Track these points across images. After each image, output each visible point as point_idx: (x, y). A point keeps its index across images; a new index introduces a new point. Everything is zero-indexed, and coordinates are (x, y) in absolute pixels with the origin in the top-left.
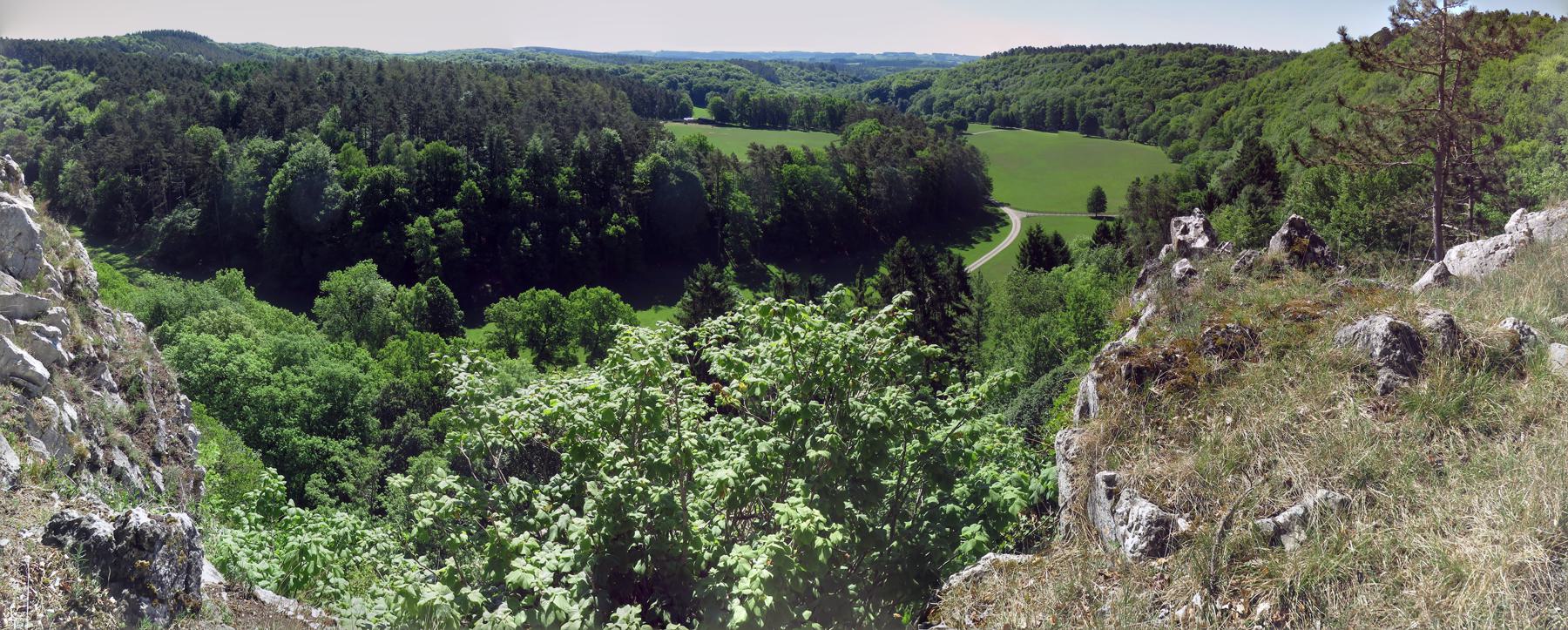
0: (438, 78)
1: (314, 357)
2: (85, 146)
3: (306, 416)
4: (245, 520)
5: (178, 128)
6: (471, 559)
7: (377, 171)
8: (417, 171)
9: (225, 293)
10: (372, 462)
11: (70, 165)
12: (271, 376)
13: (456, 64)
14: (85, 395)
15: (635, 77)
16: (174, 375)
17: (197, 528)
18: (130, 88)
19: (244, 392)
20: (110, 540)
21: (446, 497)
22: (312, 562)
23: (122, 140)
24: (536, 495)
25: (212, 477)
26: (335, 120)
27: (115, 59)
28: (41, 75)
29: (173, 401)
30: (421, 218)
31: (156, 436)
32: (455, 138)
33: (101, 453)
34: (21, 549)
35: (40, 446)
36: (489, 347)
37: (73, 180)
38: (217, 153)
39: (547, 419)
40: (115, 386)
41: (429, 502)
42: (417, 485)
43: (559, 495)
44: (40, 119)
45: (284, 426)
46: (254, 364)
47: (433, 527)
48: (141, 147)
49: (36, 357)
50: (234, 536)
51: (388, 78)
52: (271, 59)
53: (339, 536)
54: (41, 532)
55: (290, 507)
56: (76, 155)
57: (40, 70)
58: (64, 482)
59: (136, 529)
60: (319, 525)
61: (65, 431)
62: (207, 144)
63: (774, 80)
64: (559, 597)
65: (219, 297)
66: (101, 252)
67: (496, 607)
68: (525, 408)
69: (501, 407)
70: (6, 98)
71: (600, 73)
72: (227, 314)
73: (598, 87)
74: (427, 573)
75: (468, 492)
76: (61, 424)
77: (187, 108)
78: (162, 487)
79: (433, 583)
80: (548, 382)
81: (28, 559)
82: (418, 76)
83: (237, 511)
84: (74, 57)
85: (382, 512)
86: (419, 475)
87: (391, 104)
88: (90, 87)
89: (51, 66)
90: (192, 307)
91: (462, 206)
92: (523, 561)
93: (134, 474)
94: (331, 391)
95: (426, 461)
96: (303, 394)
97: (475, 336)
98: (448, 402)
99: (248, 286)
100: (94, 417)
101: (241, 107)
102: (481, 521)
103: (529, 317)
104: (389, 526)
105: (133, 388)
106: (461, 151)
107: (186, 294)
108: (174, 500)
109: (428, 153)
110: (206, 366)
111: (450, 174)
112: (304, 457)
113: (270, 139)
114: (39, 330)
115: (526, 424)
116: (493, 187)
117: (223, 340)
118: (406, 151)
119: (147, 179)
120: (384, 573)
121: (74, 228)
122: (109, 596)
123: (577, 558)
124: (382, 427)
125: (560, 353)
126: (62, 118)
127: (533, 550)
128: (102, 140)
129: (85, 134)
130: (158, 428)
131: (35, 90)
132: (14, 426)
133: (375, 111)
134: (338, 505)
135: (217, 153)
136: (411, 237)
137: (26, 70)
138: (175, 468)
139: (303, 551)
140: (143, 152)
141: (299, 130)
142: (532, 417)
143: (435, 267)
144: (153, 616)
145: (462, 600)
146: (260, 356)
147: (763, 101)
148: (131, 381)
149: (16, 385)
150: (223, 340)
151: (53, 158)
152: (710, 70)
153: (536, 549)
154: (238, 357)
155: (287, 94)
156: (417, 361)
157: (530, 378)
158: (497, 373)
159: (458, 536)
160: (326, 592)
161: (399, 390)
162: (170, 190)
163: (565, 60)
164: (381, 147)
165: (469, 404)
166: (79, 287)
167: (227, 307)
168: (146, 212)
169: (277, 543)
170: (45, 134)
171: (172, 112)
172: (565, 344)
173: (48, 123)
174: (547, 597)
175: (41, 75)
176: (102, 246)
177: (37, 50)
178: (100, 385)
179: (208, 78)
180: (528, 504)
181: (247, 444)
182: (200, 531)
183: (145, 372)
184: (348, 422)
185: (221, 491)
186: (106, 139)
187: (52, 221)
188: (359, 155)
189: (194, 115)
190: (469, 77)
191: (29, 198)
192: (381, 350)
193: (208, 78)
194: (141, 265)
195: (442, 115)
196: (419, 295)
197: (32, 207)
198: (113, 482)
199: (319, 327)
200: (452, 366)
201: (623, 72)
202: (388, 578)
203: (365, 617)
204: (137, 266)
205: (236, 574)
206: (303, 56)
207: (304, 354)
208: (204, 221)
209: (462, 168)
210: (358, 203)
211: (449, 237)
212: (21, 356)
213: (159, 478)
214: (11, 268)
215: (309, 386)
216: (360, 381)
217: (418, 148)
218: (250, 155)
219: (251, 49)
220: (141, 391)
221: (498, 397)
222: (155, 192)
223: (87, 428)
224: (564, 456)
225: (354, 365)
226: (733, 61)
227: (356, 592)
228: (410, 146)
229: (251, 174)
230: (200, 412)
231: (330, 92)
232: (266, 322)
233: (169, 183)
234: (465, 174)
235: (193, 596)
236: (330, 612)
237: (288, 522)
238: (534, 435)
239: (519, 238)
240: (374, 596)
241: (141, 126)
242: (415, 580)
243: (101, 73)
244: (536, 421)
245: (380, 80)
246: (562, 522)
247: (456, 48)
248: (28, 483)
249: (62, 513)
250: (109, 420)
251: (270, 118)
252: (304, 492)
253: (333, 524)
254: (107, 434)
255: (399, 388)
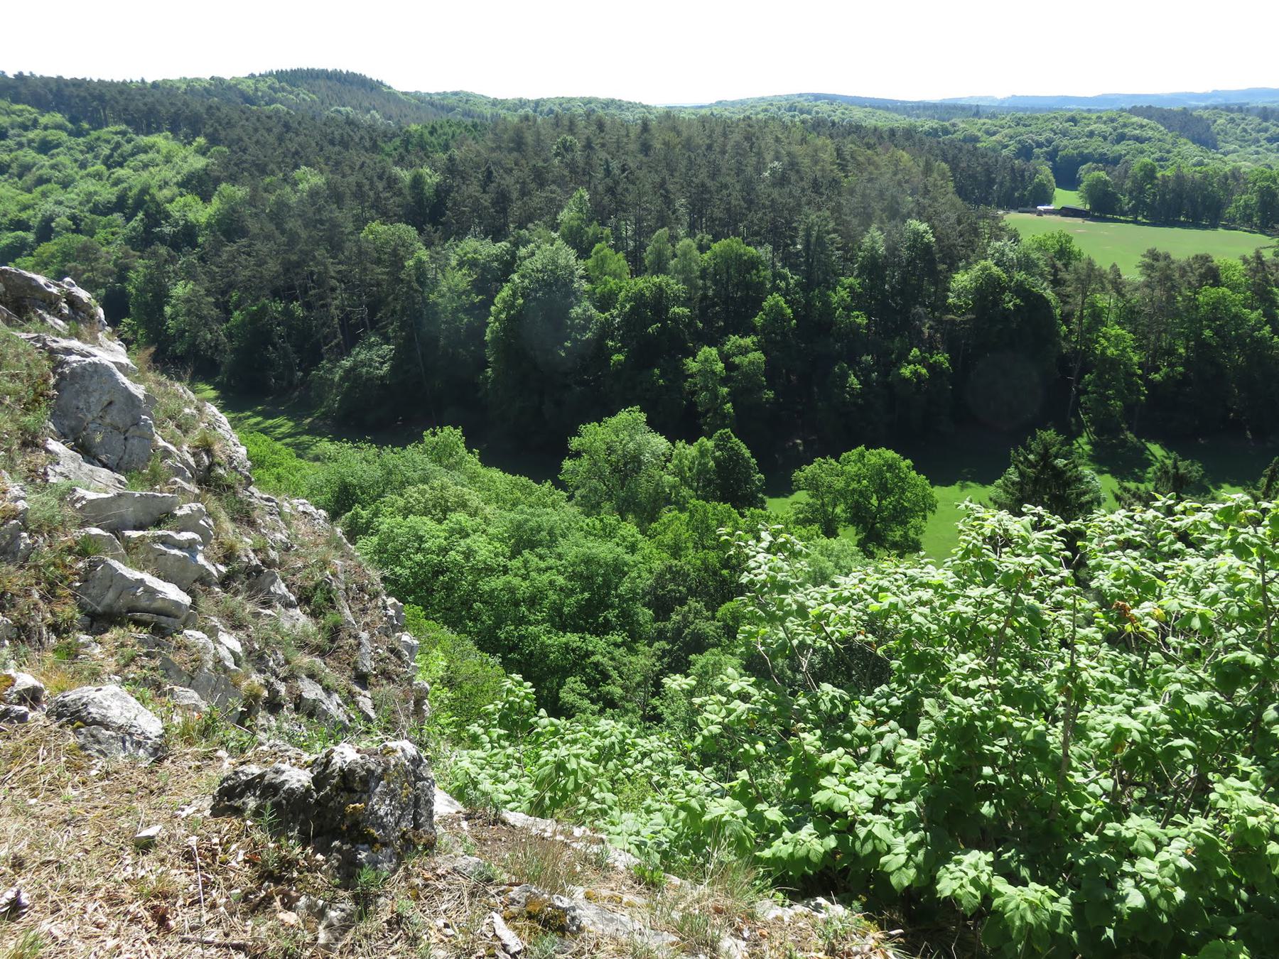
0: (730, 144)
1: (564, 536)
2: (202, 259)
3: (557, 609)
4: (485, 738)
5: (350, 227)
6: (769, 774)
7: (643, 284)
8: (700, 282)
9: (438, 460)
10: (643, 661)
11: (180, 290)
12: (509, 563)
13: (758, 121)
14: (250, 618)
15: (965, 140)
16: (375, 575)
17: (423, 755)
18: (266, 165)
19: (474, 586)
20: (308, 790)
21: (738, 702)
22: (572, 778)
23: (262, 247)
24: (854, 708)
25: (438, 693)
26: (581, 210)
27: (235, 116)
28: (108, 142)
29: (377, 607)
30: (706, 348)
31: (358, 654)
32: (757, 234)
33: (282, 688)
34: (181, 832)
35: (190, 696)
36: (797, 522)
37: (189, 313)
38: (411, 263)
39: (874, 617)
40: (293, 598)
41: (717, 708)
42: (702, 687)
43: (885, 709)
44: (117, 217)
45: (529, 623)
46: (484, 549)
47: (721, 735)
48: (294, 258)
49: (166, 579)
50: (472, 758)
51: (657, 145)
52: (481, 116)
53: (604, 747)
54: (208, 803)
55: (541, 717)
56: (188, 273)
57: (105, 132)
58: (233, 734)
59: (341, 769)
60: (578, 735)
61: (226, 669)
62: (395, 250)
63: (1206, 140)
64: (879, 825)
65: (430, 466)
66: (248, 417)
67: (800, 828)
68: (845, 601)
69: (812, 598)
70: (48, 181)
71: (909, 133)
72: (443, 488)
73: (906, 156)
74: (714, 786)
75: (767, 697)
76: (219, 661)
77: (359, 194)
78: (372, 714)
79: (722, 797)
80: (877, 570)
81: (193, 841)
82: (702, 141)
83: (474, 728)
84: (163, 112)
85: (658, 718)
86: (704, 676)
87: (663, 184)
88: (199, 163)
89: (123, 127)
90: (393, 482)
91: (764, 331)
92: (835, 780)
93: (333, 705)
94: (588, 578)
95: (712, 659)
96: (551, 583)
97: (778, 507)
98: (741, 590)
99: (469, 449)
100: (267, 644)
101: (442, 192)
102: (782, 732)
103: (854, 485)
104: (666, 734)
105: (318, 597)
106: (764, 252)
107: (383, 466)
108: (391, 727)
109: (715, 256)
110: (419, 557)
111: (748, 286)
112: (556, 658)
113: (488, 240)
114: (165, 541)
115: (845, 620)
116: (809, 305)
117: (440, 522)
118: (685, 254)
119: (308, 306)
120: (659, 786)
121: (201, 386)
122: (315, 853)
123: (905, 786)
124: (656, 620)
125: (897, 534)
126: (157, 215)
127: (848, 770)
128: (230, 248)
129: (200, 240)
130: (360, 644)
131: (100, 167)
132: (145, 679)
133: (640, 195)
134: (601, 712)
135: (411, 263)
136: (692, 376)
137: (79, 133)
138: (388, 689)
139: (560, 766)
140: (298, 264)
141: (530, 225)
142: (853, 613)
143: (725, 416)
144: (375, 864)
145: (758, 818)
146: (492, 539)
147: (1180, 178)
148: (315, 588)
149: (137, 623)
150: (440, 522)
151: (149, 280)
152: (1091, 128)
153: (853, 769)
154: (462, 542)
155: (509, 171)
156: (701, 538)
157: (853, 564)
158: (808, 555)
159: (753, 747)
160: (590, 808)
161: (677, 575)
162: (345, 321)
163: (858, 114)
164: (649, 249)
165: (770, 592)
166: (221, 471)
167: (442, 478)
168: (312, 356)
169: (526, 760)
170: (129, 241)
171: (337, 202)
172: (904, 523)
173: (133, 223)
174: (864, 823)
175: (108, 142)
176: (249, 409)
177: (94, 98)
178: (271, 601)
179: (388, 148)
180: (844, 716)
181: (481, 648)
182: (427, 758)
183: (334, 575)
184: (611, 615)
185: (451, 708)
186: (235, 247)
187: (163, 378)
188: (618, 261)
189: (372, 207)
190: (777, 140)
191: (118, 346)
192: (653, 525)
193: (388, 148)
194: (312, 431)
195: (736, 200)
196: (703, 453)
197: (124, 359)
198: (304, 720)
199: (570, 498)
200: (747, 545)
201: (946, 132)
202: (666, 792)
203: (638, 833)
204: (307, 432)
205: (477, 799)
206: (531, 112)
207: (551, 533)
208: (399, 362)
209: (765, 278)
210: (618, 329)
211: (746, 375)
212: (141, 581)
213: (366, 703)
214: (103, 458)
215: (559, 573)
216: (626, 564)
217: (702, 248)
218: (461, 264)
219: (452, 101)
220: (331, 600)
221: (808, 585)
222: (324, 324)
223: (258, 660)
224: (895, 664)
225: (618, 545)
226: (1135, 111)
227: (626, 807)
228: (689, 246)
229: (464, 292)
230: (415, 616)
231: (572, 167)
232: (497, 495)
233: (343, 310)
234: (769, 286)
235: (425, 832)
236: (595, 830)
237: (539, 735)
238: (855, 635)
239: (844, 376)
240: (648, 811)
241: (290, 224)
242: (699, 793)
243: (213, 140)
244: (859, 618)
245: (646, 148)
246: (888, 741)
247: (758, 95)
248: (179, 748)
249: (236, 773)
250: (289, 644)
251: (485, 208)
252: (559, 699)
253: (596, 734)
254: (287, 662)
255: (678, 572)
